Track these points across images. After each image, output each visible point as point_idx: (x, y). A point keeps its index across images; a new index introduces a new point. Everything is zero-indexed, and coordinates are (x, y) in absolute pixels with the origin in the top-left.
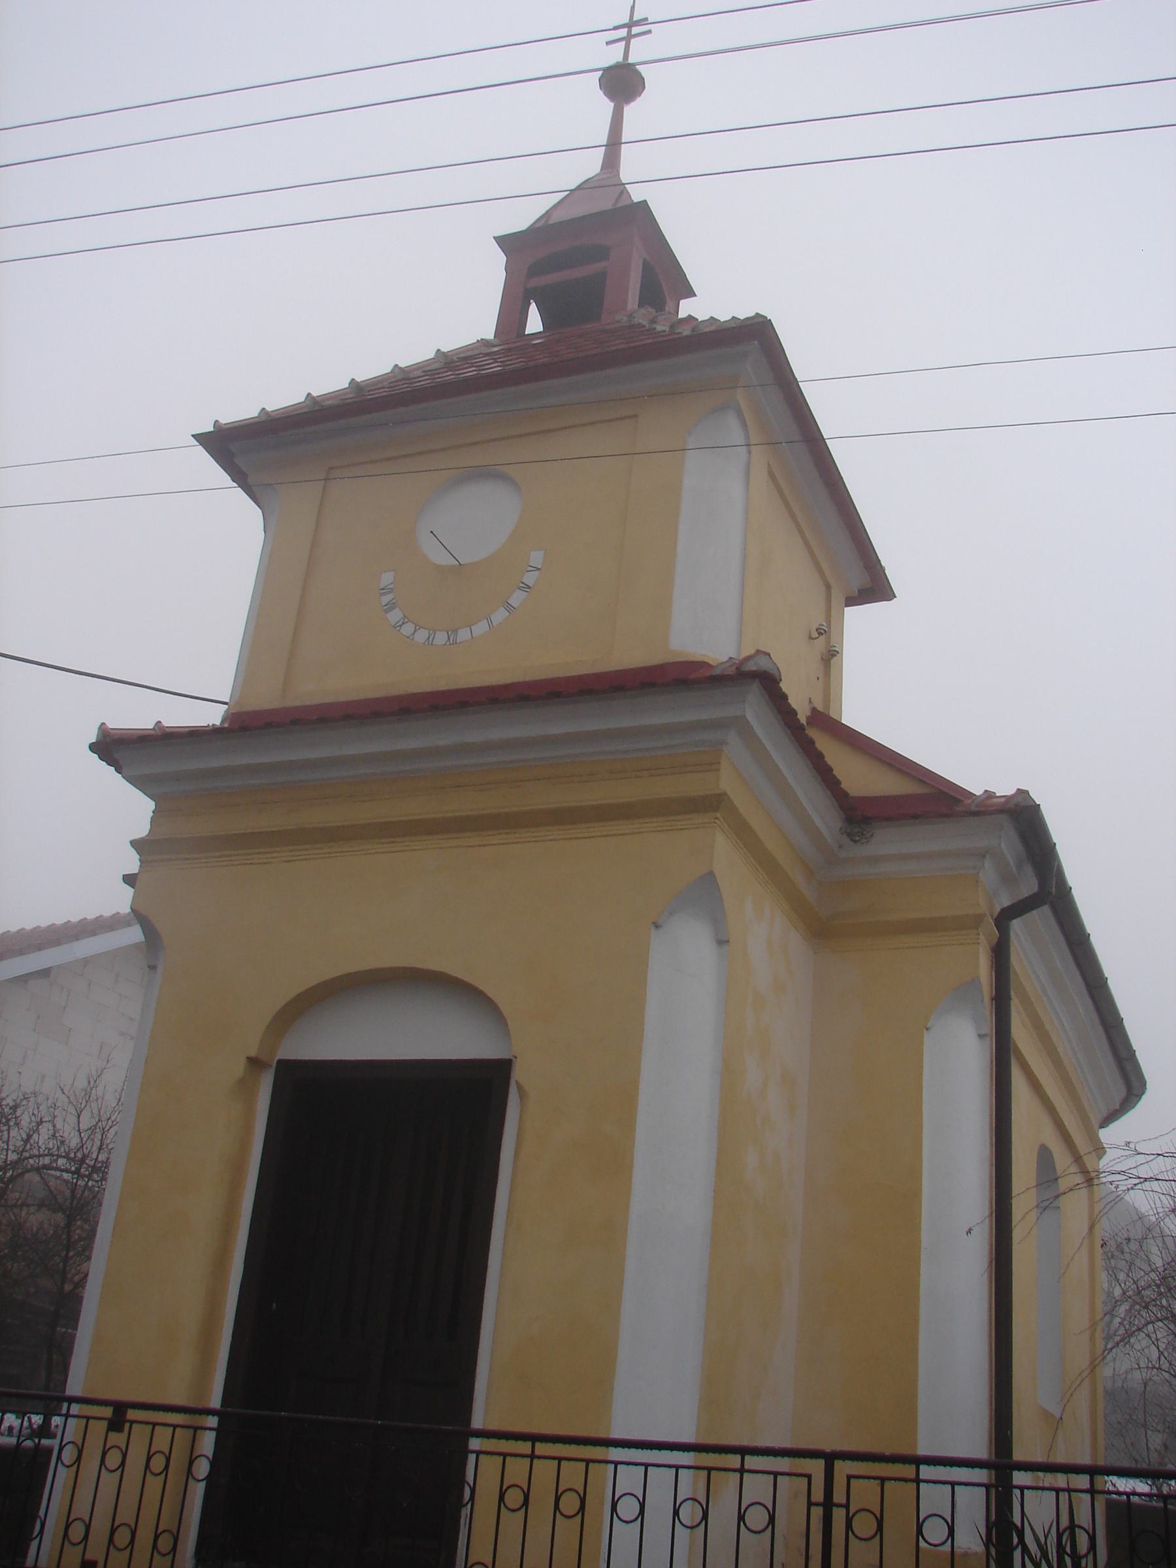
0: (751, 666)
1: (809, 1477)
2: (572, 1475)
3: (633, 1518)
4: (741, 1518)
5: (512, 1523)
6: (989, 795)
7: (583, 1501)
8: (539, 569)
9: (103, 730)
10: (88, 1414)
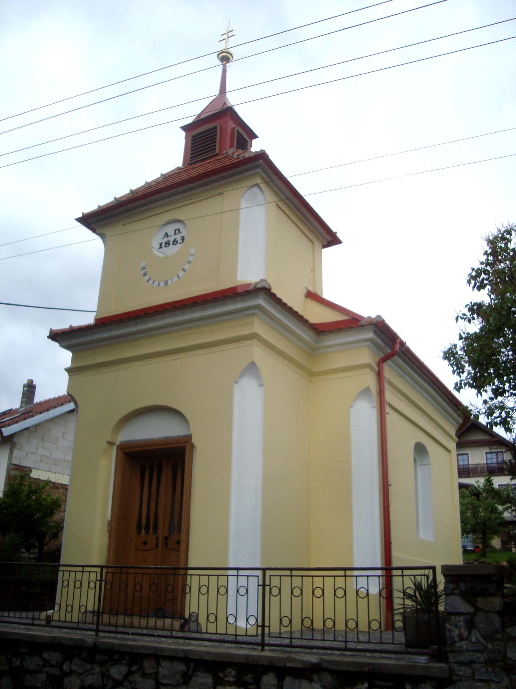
0: (259, 286)
1: (258, 576)
2: (340, 582)
3: (320, 596)
4: (238, 591)
5: (242, 600)
6: (369, 318)
7: (302, 591)
8: (193, 255)
9: (51, 331)
10: (70, 570)
